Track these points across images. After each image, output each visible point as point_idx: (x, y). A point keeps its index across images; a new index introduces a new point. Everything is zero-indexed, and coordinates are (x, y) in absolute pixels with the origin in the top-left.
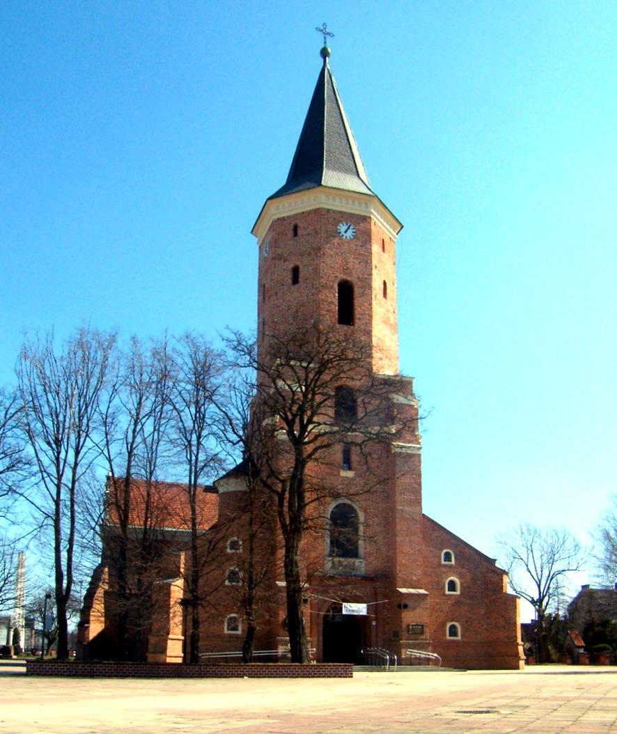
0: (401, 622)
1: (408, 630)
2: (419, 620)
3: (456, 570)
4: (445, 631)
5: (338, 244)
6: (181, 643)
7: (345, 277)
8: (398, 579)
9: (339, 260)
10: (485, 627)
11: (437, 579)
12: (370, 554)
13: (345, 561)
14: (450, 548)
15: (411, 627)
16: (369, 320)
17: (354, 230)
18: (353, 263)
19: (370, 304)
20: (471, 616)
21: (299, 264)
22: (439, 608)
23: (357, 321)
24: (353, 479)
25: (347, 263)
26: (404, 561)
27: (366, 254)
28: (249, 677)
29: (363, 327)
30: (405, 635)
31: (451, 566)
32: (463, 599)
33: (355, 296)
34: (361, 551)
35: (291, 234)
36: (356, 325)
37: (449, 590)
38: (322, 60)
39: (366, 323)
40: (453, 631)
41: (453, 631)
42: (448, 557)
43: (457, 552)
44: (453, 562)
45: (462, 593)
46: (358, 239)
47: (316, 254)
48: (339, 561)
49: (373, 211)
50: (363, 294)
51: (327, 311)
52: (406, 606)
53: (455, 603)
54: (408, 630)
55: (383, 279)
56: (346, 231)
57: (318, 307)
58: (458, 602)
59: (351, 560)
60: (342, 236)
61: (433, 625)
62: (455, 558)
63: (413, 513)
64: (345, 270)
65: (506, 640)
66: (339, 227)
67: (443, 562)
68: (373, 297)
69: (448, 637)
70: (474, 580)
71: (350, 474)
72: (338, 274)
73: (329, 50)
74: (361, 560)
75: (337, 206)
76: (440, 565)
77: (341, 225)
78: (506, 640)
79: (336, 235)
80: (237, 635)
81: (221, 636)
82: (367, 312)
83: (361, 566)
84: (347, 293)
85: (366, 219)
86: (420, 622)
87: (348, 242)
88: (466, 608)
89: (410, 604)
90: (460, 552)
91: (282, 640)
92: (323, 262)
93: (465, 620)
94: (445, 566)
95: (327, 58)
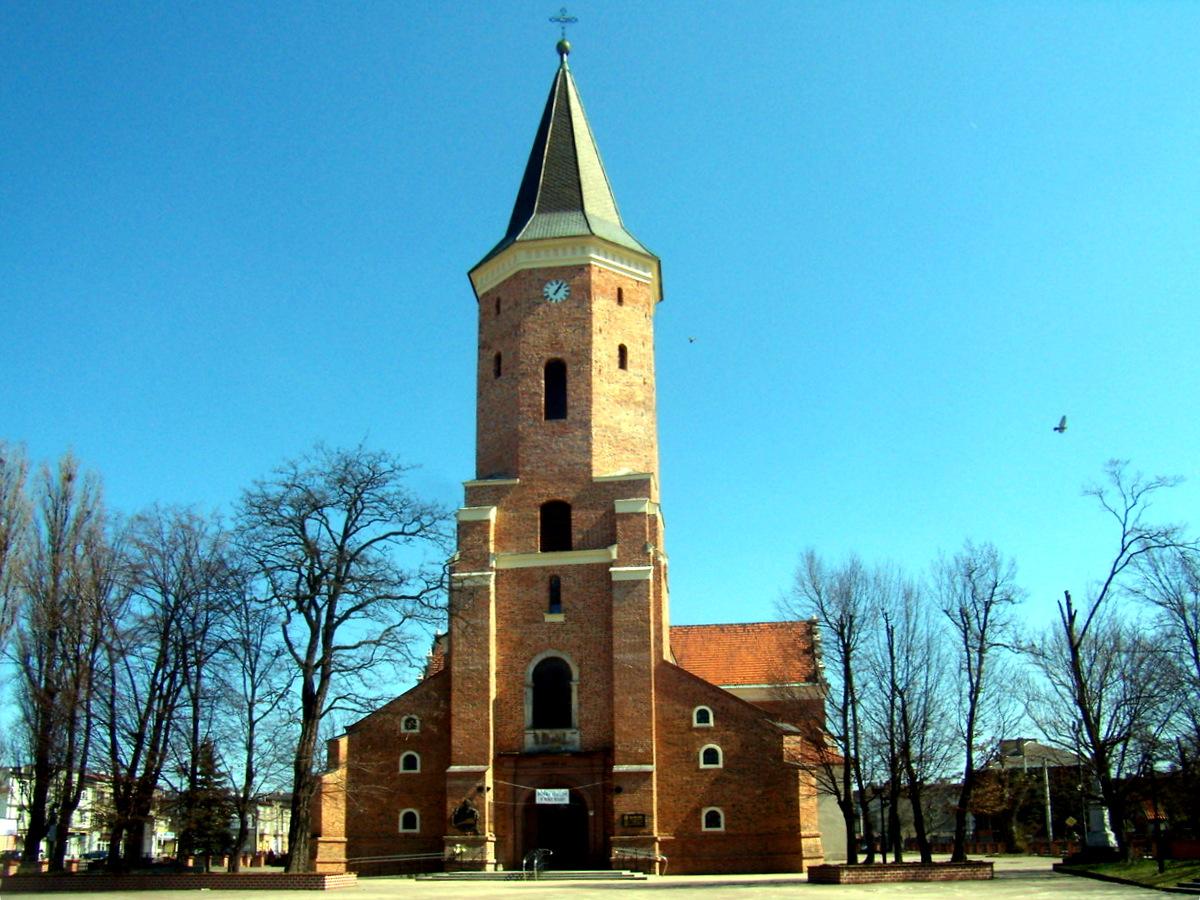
0: (613, 812)
1: (623, 821)
2: (639, 808)
3: (715, 734)
4: (700, 820)
5: (544, 312)
6: (343, 846)
7: (552, 355)
8: (617, 753)
9: (545, 334)
10: (764, 812)
11: (686, 749)
12: (587, 721)
13: (552, 733)
14: (706, 704)
15: (626, 818)
16: (587, 406)
17: (567, 288)
18: (566, 333)
19: (589, 385)
20: (741, 797)
21: (501, 350)
22: (691, 789)
23: (570, 411)
24: (563, 624)
25: (557, 335)
26: (624, 729)
27: (584, 316)
28: (211, 889)
29: (578, 417)
30: (618, 828)
31: (708, 729)
32: (727, 775)
33: (568, 378)
34: (575, 719)
35: (493, 310)
36: (569, 418)
37: (717, 763)
38: (558, 57)
39: (583, 412)
40: (713, 820)
41: (713, 820)
42: (703, 716)
43: (719, 709)
44: (712, 723)
45: (725, 765)
46: (573, 299)
47: (516, 334)
48: (544, 735)
49: (593, 255)
50: (579, 373)
51: (529, 406)
52: (619, 790)
53: (716, 780)
54: (623, 821)
55: (620, 342)
56: (556, 293)
57: (518, 405)
58: (719, 779)
59: (559, 732)
60: (551, 300)
61: (682, 812)
62: (714, 716)
63: (638, 661)
64: (555, 344)
65: (787, 829)
66: (546, 290)
67: (695, 724)
68: (594, 372)
69: (704, 829)
70: (744, 746)
71: (559, 618)
72: (545, 354)
73: (568, 44)
74: (574, 730)
75: (569, 260)
76: (691, 729)
77: (549, 285)
78: (787, 829)
79: (541, 300)
80: (720, 832)
81: (395, 836)
82: (583, 396)
83: (573, 737)
84: (557, 377)
85: (583, 269)
86: (642, 810)
87: (558, 308)
88: (732, 786)
89: (625, 786)
90: (723, 708)
91: (449, 840)
92: (524, 342)
93: (731, 803)
94: (698, 730)
95: (565, 56)
